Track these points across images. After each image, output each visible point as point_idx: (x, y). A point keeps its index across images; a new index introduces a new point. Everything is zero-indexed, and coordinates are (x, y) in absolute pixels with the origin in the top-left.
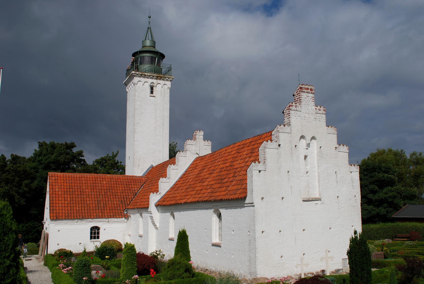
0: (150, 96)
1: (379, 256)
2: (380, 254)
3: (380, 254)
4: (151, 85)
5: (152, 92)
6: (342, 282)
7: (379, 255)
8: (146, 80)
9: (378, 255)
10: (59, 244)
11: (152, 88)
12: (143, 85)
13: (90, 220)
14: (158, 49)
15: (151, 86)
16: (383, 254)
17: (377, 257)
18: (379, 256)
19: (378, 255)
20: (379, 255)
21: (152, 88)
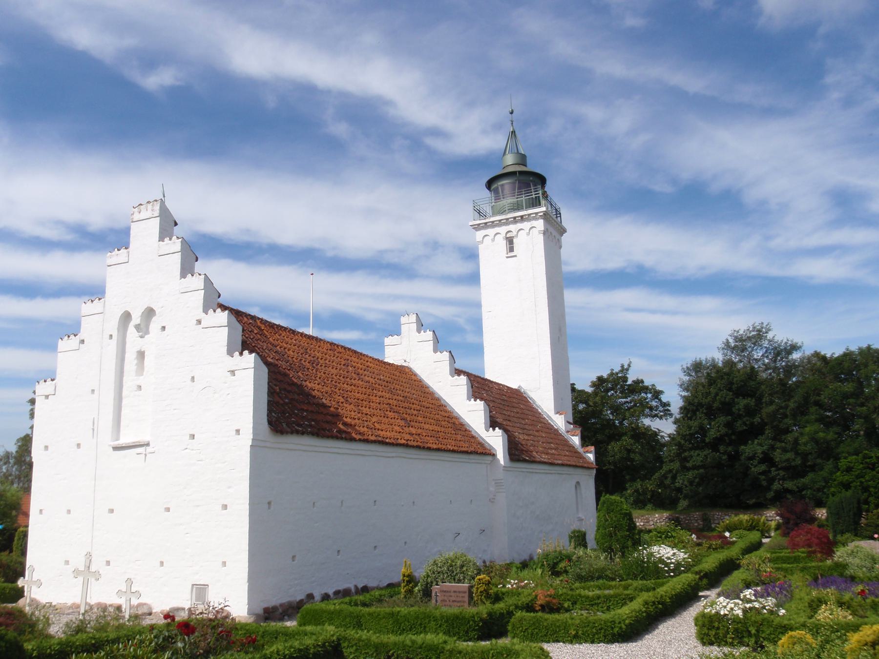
0: (507, 257)
1: (451, 596)
2: (455, 592)
3: (455, 590)
4: (508, 236)
5: (511, 249)
6: (632, 441)
7: (452, 594)
8: (497, 230)
9: (448, 594)
10: (169, 511)
11: (510, 241)
12: (493, 240)
13: (316, 446)
14: (532, 166)
15: (507, 238)
16: (465, 592)
17: (446, 598)
18: (451, 596)
19: (450, 592)
20: (452, 594)
21: (510, 241)
